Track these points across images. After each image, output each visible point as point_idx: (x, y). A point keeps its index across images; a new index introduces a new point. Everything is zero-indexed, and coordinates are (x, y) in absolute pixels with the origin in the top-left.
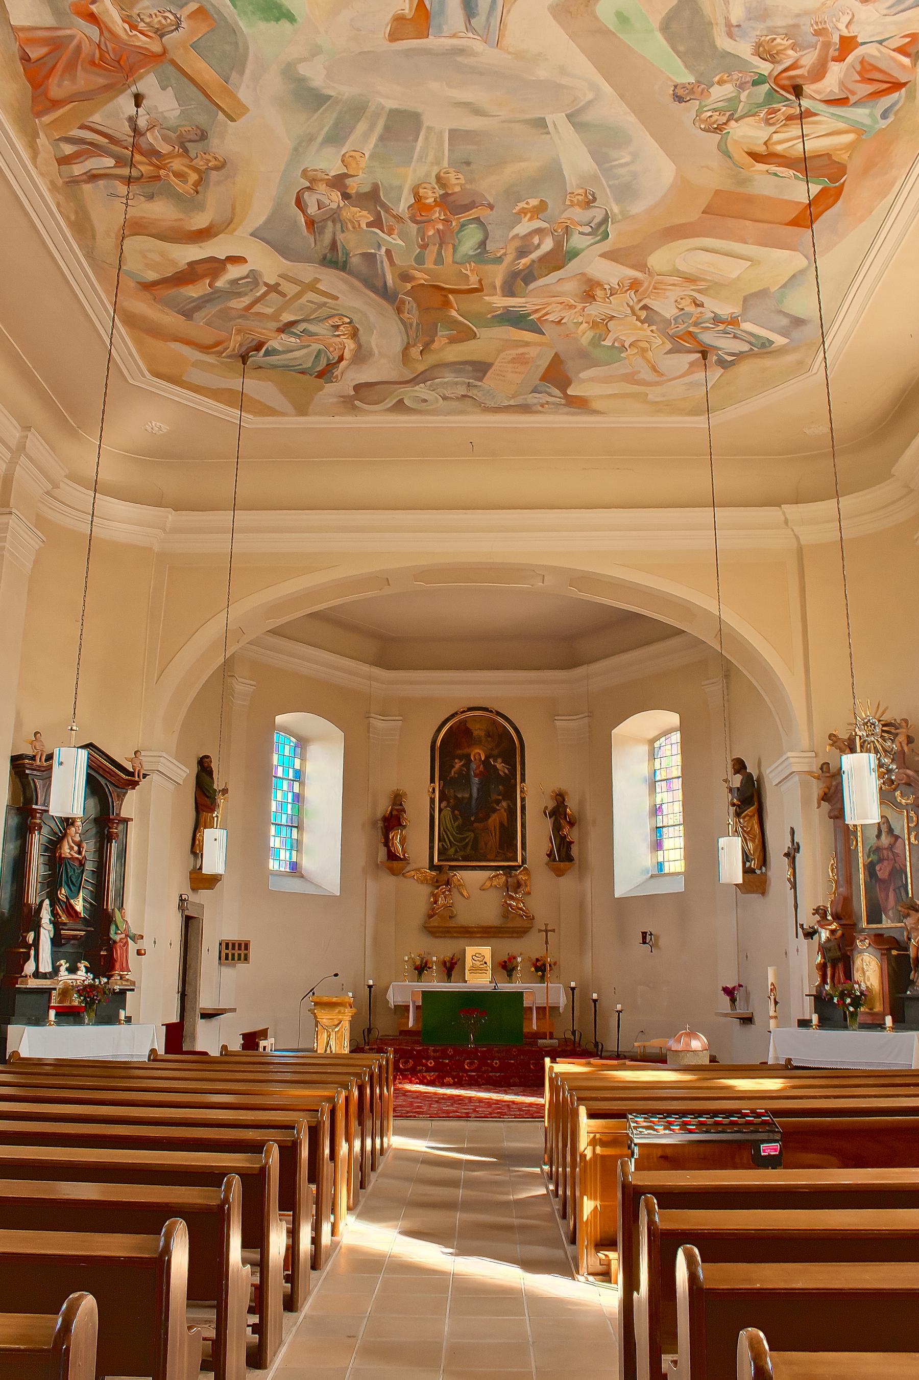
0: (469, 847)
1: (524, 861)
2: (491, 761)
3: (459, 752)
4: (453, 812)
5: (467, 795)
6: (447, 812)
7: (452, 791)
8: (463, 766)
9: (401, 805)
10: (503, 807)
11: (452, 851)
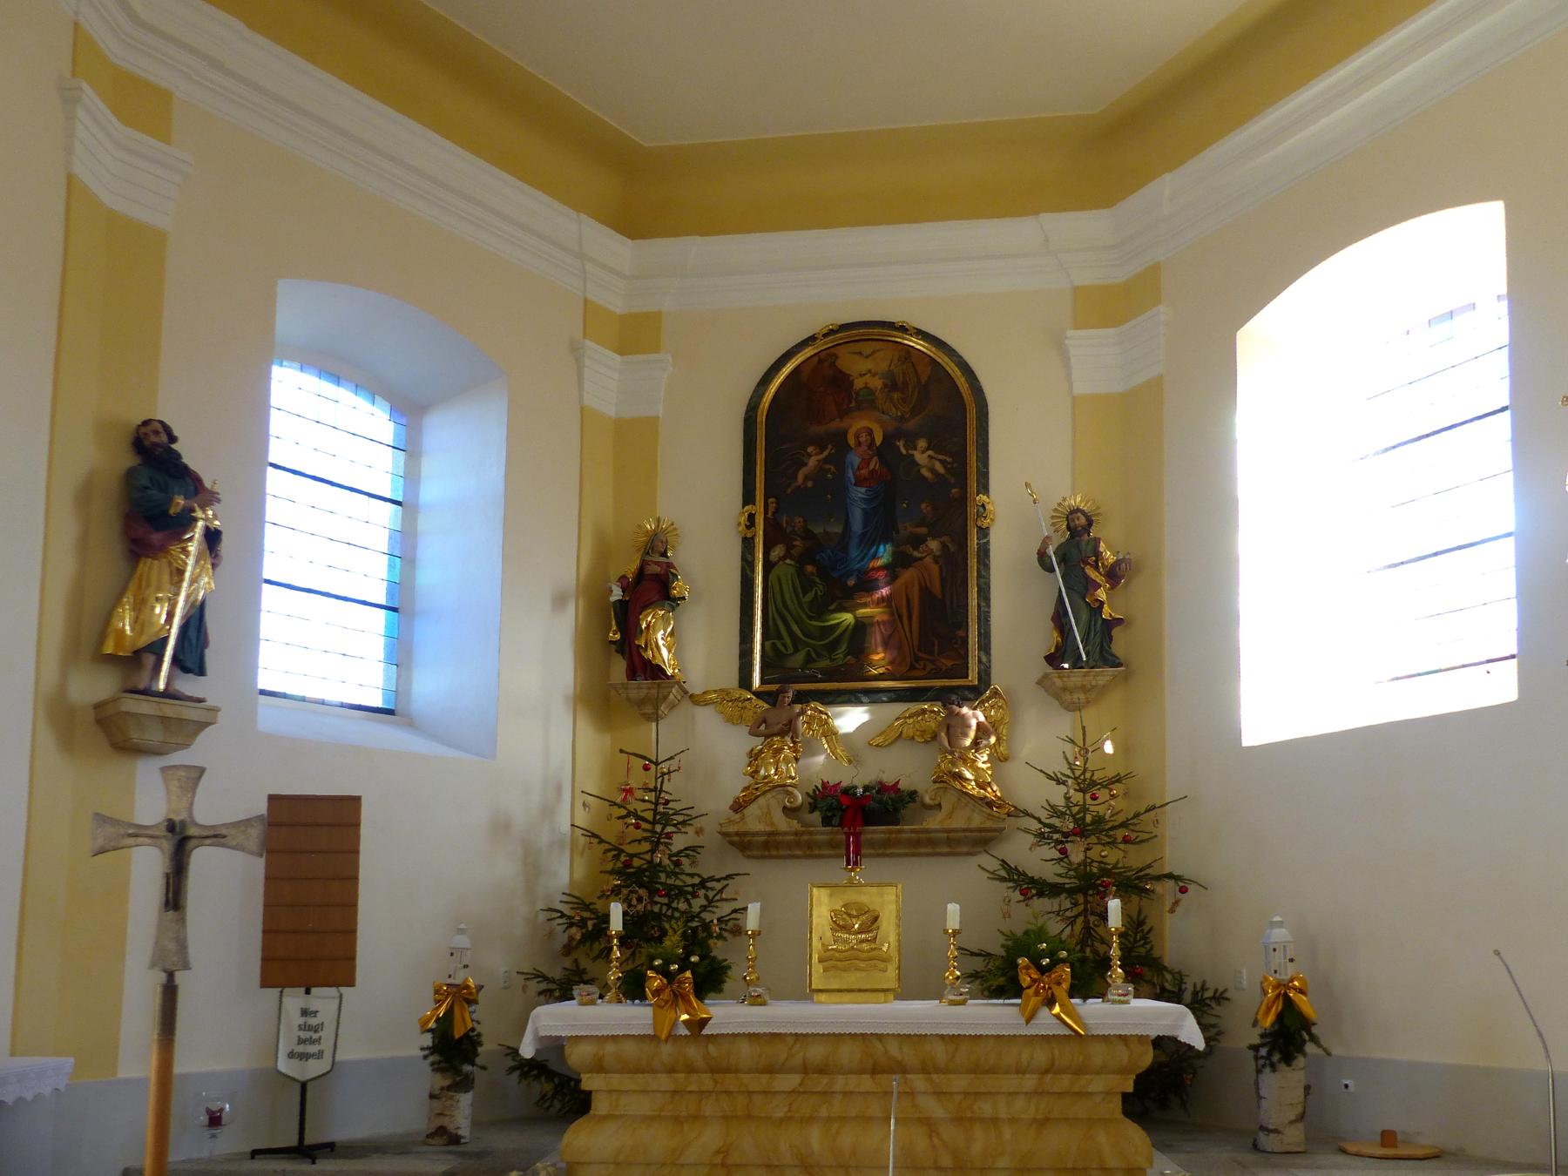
2: (901, 444)
5: (838, 529)
6: (786, 570)
7: (798, 520)
8: (825, 461)
9: (664, 554)
10: (930, 552)
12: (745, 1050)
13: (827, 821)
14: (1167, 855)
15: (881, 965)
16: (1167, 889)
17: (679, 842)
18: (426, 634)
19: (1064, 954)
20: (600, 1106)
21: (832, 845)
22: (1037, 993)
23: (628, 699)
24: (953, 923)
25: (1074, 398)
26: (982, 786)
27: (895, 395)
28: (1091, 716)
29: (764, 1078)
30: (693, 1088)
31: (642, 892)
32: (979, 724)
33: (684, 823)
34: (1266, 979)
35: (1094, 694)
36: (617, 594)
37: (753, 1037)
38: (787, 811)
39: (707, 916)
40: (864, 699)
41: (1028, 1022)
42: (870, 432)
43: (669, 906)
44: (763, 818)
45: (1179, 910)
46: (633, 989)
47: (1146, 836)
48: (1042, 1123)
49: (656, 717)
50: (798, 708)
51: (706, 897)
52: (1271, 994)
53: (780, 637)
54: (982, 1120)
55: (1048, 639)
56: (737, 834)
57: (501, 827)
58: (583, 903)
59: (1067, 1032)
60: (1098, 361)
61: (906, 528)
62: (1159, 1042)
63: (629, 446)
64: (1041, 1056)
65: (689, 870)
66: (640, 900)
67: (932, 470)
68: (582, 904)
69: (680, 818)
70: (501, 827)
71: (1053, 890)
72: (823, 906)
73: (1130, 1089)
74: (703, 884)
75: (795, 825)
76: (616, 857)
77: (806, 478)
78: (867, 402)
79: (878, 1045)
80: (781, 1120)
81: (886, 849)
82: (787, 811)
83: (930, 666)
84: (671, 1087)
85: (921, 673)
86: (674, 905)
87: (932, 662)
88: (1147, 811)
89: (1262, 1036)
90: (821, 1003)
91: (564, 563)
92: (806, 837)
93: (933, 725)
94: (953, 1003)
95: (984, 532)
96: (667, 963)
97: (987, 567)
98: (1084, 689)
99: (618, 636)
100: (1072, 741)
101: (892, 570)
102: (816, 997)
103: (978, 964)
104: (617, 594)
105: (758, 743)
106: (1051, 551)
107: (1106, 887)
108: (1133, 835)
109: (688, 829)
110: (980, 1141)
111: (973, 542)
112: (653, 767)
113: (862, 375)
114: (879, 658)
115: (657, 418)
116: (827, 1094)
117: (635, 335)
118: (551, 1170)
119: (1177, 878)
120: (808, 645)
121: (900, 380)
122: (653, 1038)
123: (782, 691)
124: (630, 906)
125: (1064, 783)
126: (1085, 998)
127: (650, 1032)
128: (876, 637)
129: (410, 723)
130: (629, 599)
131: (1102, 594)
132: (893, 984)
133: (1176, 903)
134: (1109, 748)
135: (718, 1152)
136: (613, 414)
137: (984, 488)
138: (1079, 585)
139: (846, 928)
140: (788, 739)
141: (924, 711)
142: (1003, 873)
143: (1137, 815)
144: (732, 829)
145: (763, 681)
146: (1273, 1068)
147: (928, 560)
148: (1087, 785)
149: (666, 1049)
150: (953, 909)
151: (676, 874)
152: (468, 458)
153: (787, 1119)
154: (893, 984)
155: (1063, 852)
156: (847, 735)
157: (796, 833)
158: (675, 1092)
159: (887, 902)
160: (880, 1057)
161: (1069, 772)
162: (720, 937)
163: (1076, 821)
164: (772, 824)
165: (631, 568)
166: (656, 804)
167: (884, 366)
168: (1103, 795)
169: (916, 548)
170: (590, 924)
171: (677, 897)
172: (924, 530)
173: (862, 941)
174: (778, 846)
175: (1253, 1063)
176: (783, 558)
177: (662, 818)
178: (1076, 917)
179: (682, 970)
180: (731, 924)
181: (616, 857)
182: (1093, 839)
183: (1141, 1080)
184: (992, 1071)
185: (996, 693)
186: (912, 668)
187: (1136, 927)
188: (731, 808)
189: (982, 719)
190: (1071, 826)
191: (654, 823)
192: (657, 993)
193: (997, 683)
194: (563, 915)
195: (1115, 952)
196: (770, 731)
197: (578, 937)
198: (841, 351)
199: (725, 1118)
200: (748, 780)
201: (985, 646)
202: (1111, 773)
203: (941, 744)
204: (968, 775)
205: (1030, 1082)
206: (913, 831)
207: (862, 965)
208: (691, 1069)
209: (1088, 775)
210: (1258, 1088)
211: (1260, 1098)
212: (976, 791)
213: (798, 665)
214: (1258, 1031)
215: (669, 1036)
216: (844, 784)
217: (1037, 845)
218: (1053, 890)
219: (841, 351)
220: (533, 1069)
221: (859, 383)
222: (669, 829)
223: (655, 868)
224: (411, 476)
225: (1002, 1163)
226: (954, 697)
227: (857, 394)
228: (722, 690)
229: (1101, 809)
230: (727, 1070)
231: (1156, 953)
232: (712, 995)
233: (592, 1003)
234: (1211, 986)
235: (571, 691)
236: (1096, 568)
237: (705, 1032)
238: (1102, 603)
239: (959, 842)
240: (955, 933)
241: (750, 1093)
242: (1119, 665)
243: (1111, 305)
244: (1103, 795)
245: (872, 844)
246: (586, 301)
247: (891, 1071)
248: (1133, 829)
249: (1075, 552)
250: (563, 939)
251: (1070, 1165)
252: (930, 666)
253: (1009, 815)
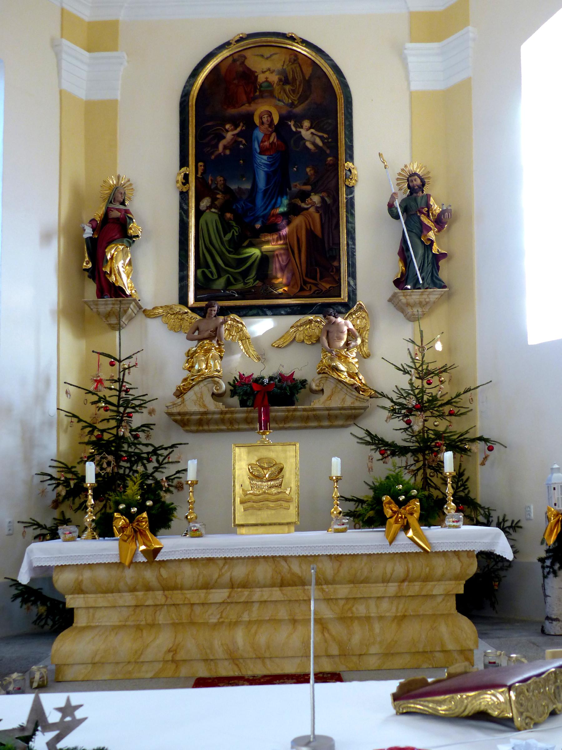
0: (253, 274)
1: (353, 294)
2: (292, 124)
3: (233, 111)
4: (221, 217)
5: (247, 186)
6: (211, 217)
7: (220, 179)
8: (238, 135)
9: (123, 203)
10: (313, 204)
11: (220, 284)
12: (188, 573)
13: (243, 404)
14: (478, 424)
15: (285, 504)
16: (478, 448)
17: (137, 420)
19: (414, 492)
20: (80, 619)
21: (247, 421)
22: (396, 522)
23: (99, 313)
25: (411, 93)
26: (351, 375)
27: (287, 87)
28: (425, 324)
29: (202, 593)
30: (150, 602)
31: (110, 458)
32: (349, 330)
33: (140, 406)
34: (549, 510)
35: (428, 308)
36: (88, 232)
37: (193, 561)
38: (217, 396)
39: (158, 475)
40: (268, 312)
41: (391, 543)
42: (270, 114)
43: (130, 468)
44: (197, 402)
45: (488, 463)
46: (104, 529)
47: (463, 410)
48: (401, 619)
49: (118, 327)
50: (221, 318)
51: (158, 461)
52: (553, 521)
53: (208, 267)
54: (359, 618)
55: (395, 268)
56: (179, 414)
58: (67, 467)
59: (419, 550)
60: (426, 67)
61: (297, 186)
62: (481, 554)
63: (96, 121)
64: (400, 569)
65: (144, 441)
66: (109, 464)
67: (314, 144)
68: (68, 469)
69: (137, 402)
71: (402, 451)
73: (462, 591)
74: (155, 452)
75: (221, 406)
76: (91, 433)
77: (225, 147)
78: (267, 92)
79: (283, 563)
80: (215, 625)
81: (285, 424)
82: (217, 396)
83: (314, 288)
84: (133, 603)
85: (307, 293)
86: (134, 468)
87: (316, 285)
88: (465, 392)
89: (547, 551)
90: (242, 534)
92: (228, 416)
93: (317, 331)
94: (337, 531)
95: (350, 190)
96: (129, 507)
97: (353, 215)
98: (421, 304)
99: (90, 265)
100: (413, 342)
102: (239, 530)
103: (351, 506)
104: (88, 232)
105: (192, 345)
106: (397, 204)
107: (439, 447)
108: (456, 410)
109: (144, 410)
110: (357, 635)
111: (343, 197)
112: (117, 363)
113: (263, 72)
114: (281, 280)
115: (116, 101)
116: (248, 603)
118: (43, 670)
119: (486, 440)
120: (228, 272)
121: (290, 77)
122: (120, 565)
123: (209, 306)
124: (102, 469)
125: (408, 373)
126: (429, 525)
127: (117, 560)
128: (276, 265)
130: (101, 232)
131: (432, 235)
132: (294, 519)
133: (486, 458)
134: (439, 346)
135: (169, 651)
136: (84, 98)
137: (350, 157)
138: (417, 229)
139: (259, 477)
140: (215, 342)
141: (310, 321)
142: (368, 439)
143: (458, 395)
144: (175, 410)
145: (196, 300)
146: (555, 574)
147: (312, 210)
148: (425, 374)
149: (129, 574)
150: (336, 462)
151: (134, 444)
153: (219, 624)
154: (294, 519)
155: (408, 422)
156: (257, 339)
157: (222, 413)
158: (136, 606)
160: (287, 575)
161: (412, 364)
162: (167, 491)
163: (417, 399)
164: (205, 406)
165: (98, 213)
166: (120, 391)
167: (278, 66)
168: (435, 381)
169: (303, 201)
170: (72, 483)
171: (136, 462)
172: (308, 188)
173: (271, 487)
174: (208, 422)
175: (540, 570)
176: (209, 208)
177: (124, 404)
178: (418, 470)
179: (139, 512)
180: (176, 481)
181: (91, 433)
182: (428, 413)
183: (469, 584)
184: (366, 581)
185: (361, 308)
186: (302, 289)
187: (460, 477)
188: (174, 394)
189: (351, 326)
190: (414, 403)
191: (118, 406)
192: (122, 529)
193: (361, 299)
194: (52, 478)
195: (449, 490)
196: (201, 336)
197: (63, 493)
198: (248, 54)
199: (174, 625)
200: (186, 374)
201: (352, 274)
202: (439, 365)
203: (323, 345)
204: (342, 367)
205: (392, 588)
206: (305, 410)
207: (271, 505)
208: (148, 588)
209: (425, 367)
210: (544, 589)
211: (546, 596)
212: (348, 380)
213: (223, 285)
214: (545, 547)
215: (131, 563)
216: (255, 376)
217: (389, 418)
218: (402, 451)
219: (248, 54)
220: (28, 594)
221: (261, 78)
222: (129, 410)
223: (119, 439)
225: (373, 650)
226: (331, 311)
227: (261, 86)
228: (166, 306)
229: (434, 392)
230: (175, 588)
231: (472, 495)
232: (162, 531)
233: (73, 539)
234: (509, 518)
235: (56, 307)
236: (428, 216)
237: (158, 559)
238: (432, 242)
239: (336, 417)
240: (338, 479)
241: (193, 604)
242: (445, 287)
244: (435, 381)
245: (276, 420)
246: (62, 9)
247: (294, 584)
248: (453, 406)
249: (413, 206)
250: (52, 496)
251: (421, 650)
252: (314, 288)
253: (371, 397)
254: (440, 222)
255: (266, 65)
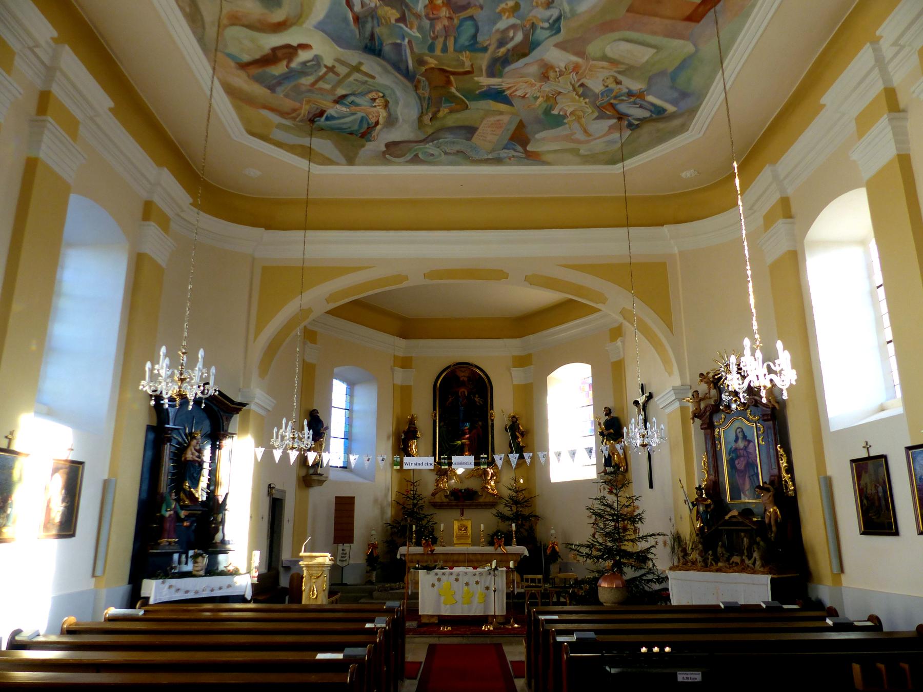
18: (355, 446)
24: (482, 528)
38: (446, 496)
46: (418, 544)
57: (376, 501)
63: (404, 394)
70: (376, 501)
72: (456, 525)
81: (470, 506)
91: (389, 428)
95: (492, 421)
101: (470, 430)
115: (410, 386)
117: (405, 363)
129: (351, 471)
131: (520, 440)
134: (522, 481)
137: (492, 409)
138: (514, 437)
149: (425, 557)
152: (367, 400)
159: (469, 524)
213: (447, 448)
224: (351, 402)
243: (523, 361)
254: (522, 434)
255: (463, 374)
